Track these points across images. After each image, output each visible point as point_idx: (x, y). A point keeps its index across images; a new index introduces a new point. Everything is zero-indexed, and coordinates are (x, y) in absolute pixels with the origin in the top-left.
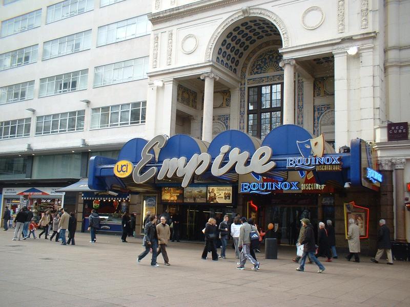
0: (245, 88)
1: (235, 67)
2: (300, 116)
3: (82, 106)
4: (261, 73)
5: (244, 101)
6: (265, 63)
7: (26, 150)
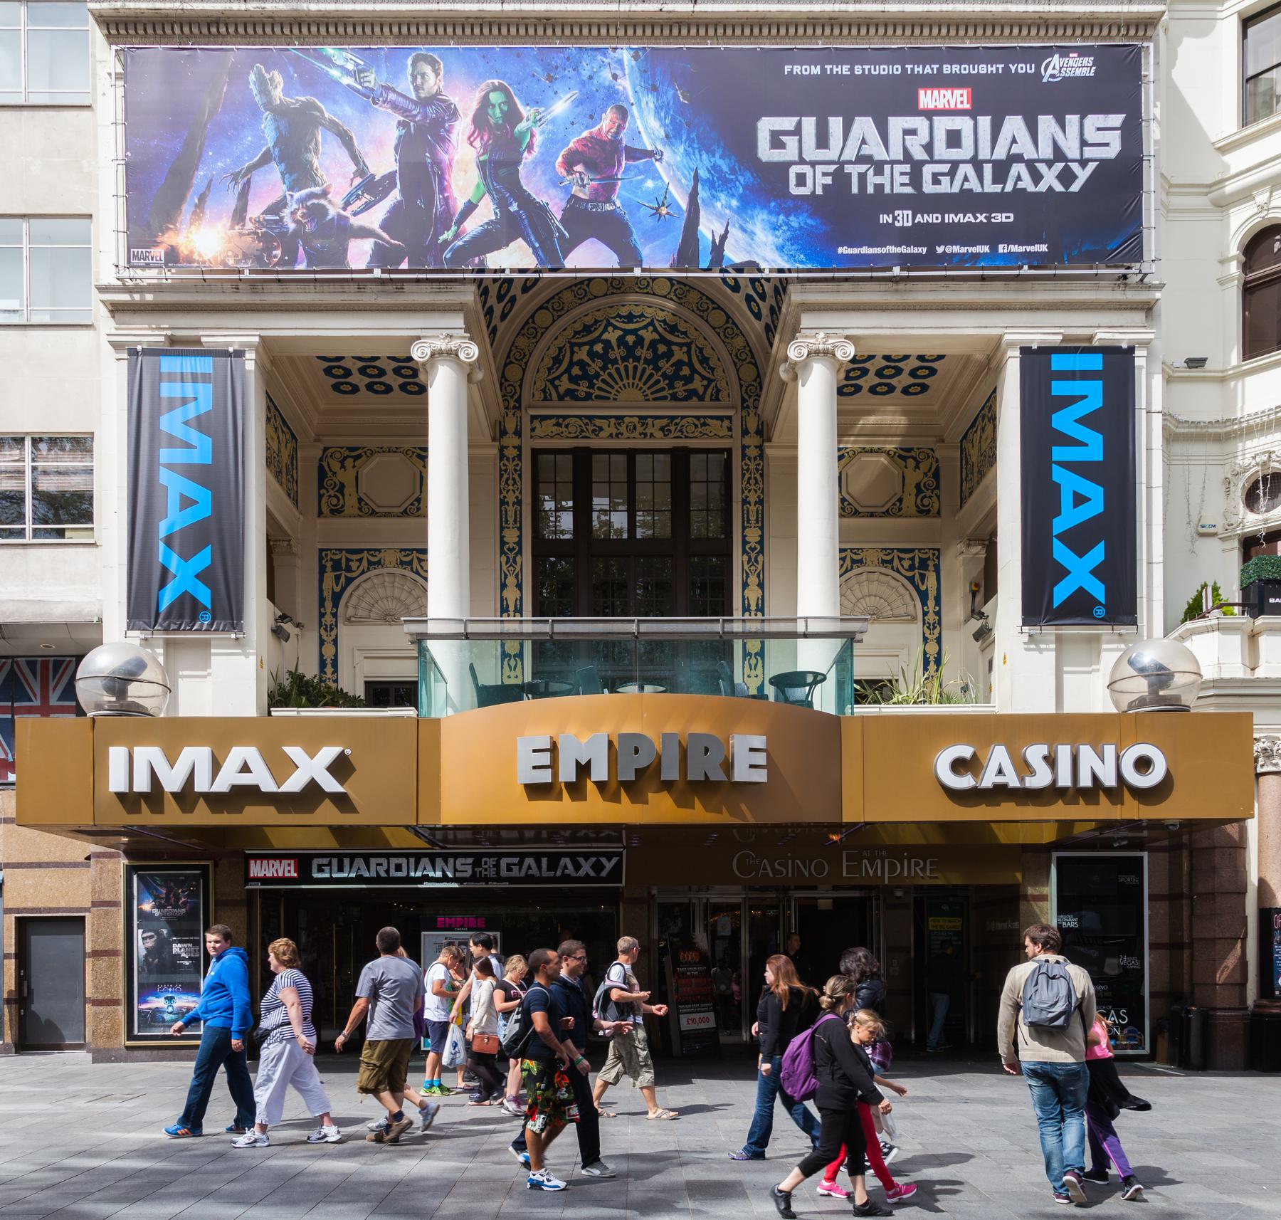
0: (519, 448)
1: (866, 387)
2: (753, 580)
4: (588, 397)
5: (519, 502)
6: (654, 361)
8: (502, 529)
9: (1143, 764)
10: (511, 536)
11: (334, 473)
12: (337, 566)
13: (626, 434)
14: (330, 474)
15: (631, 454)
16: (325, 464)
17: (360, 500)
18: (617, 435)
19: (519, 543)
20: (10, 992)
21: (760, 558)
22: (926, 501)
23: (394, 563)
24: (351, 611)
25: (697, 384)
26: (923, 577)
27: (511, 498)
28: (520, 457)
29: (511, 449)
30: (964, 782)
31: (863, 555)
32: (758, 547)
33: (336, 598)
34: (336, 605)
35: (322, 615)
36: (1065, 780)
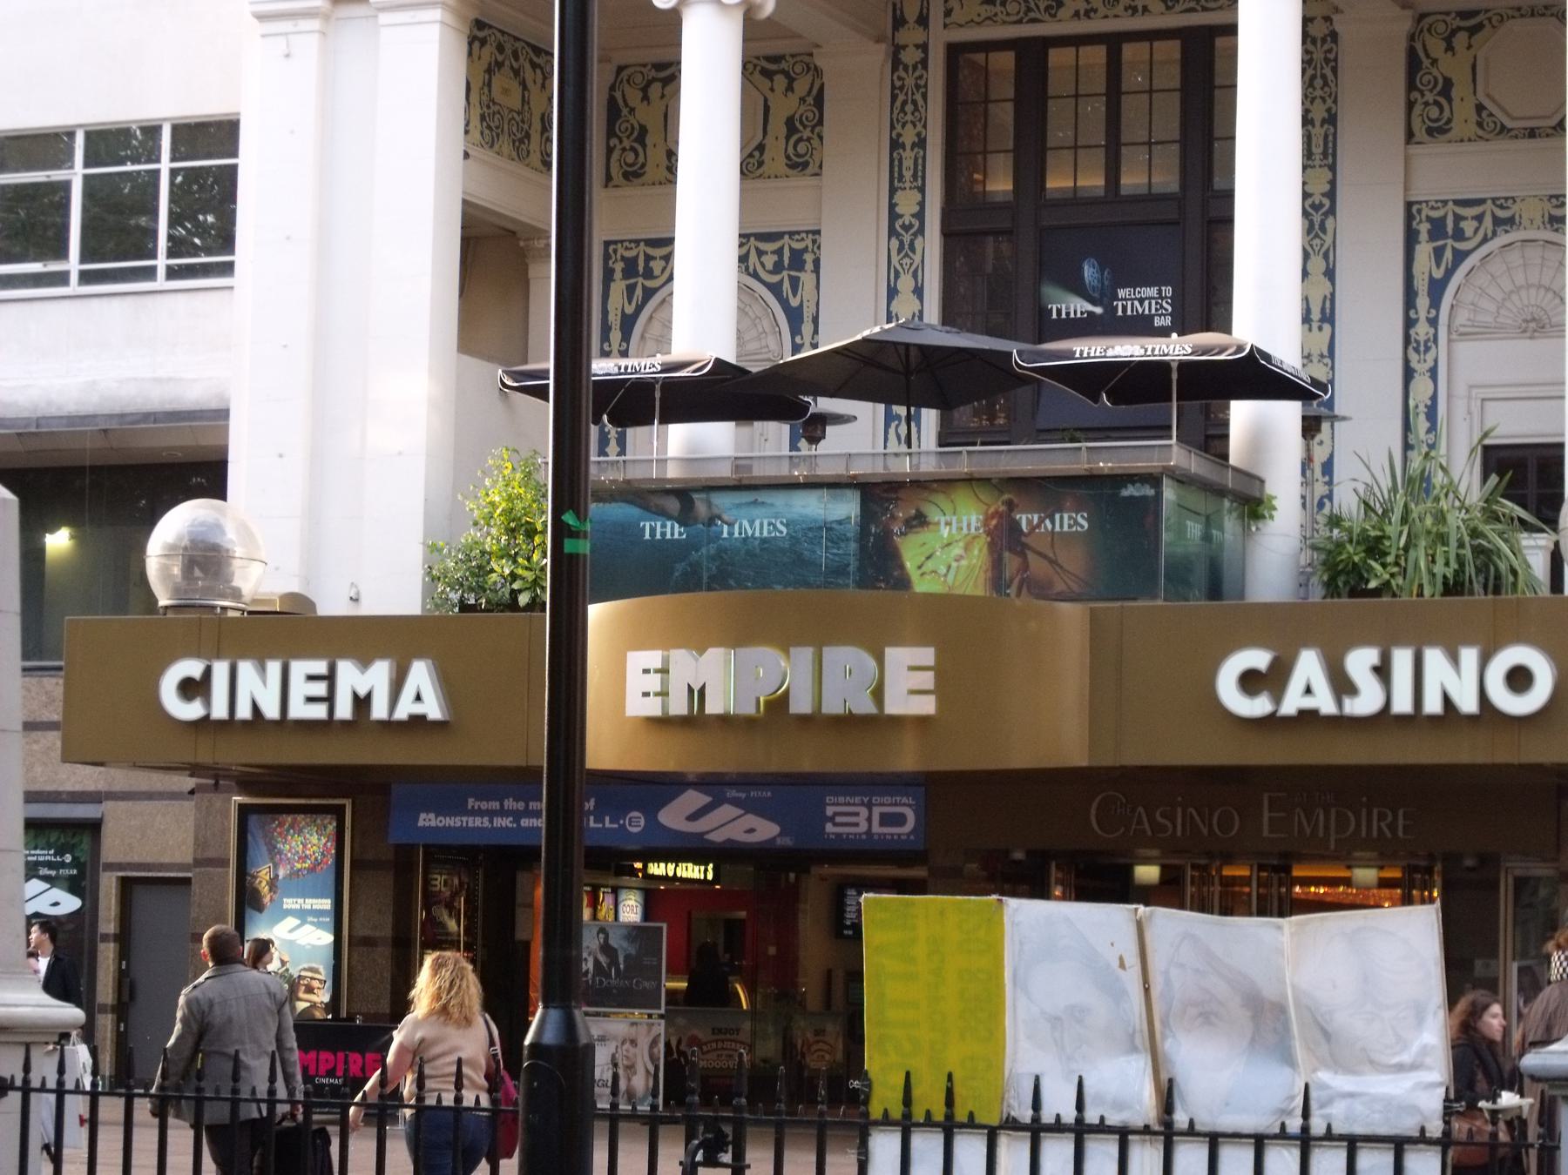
0: (924, 47)
5: (921, 143)
8: (893, 191)
11: (632, 110)
12: (630, 269)
13: (1102, 11)
14: (625, 111)
15: (1114, 42)
16: (618, 95)
17: (1480, 108)
18: (1087, 14)
19: (920, 216)
20: (509, 1155)
21: (1329, 223)
22: (802, 148)
23: (1538, 221)
24: (1462, 317)
26: (795, 283)
27: (909, 137)
28: (924, 63)
29: (911, 49)
30: (1258, 706)
31: (1515, 208)
32: (1327, 202)
33: (1437, 289)
34: (1435, 303)
35: (1409, 323)
36: (1402, 703)
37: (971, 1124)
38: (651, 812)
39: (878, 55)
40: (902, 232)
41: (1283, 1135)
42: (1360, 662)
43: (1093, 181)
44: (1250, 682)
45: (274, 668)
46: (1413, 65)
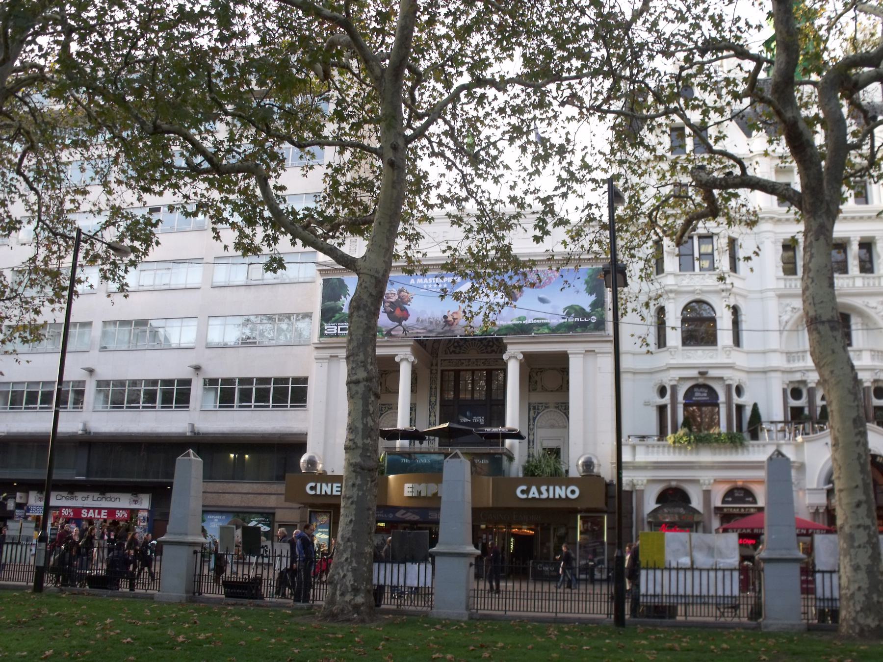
3: (184, 373)
4: (459, 353)
5: (436, 388)
7: (80, 432)
9: (573, 492)
10: (433, 399)
12: (534, 408)
15: (473, 371)
25: (495, 348)
27: (433, 387)
30: (524, 496)
33: (534, 419)
36: (551, 496)
37: (659, 568)
38: (394, 513)
39: (428, 371)
40: (432, 405)
41: (712, 569)
42: (543, 488)
43: (469, 397)
44: (523, 492)
45: (330, 485)
46: (530, 377)
